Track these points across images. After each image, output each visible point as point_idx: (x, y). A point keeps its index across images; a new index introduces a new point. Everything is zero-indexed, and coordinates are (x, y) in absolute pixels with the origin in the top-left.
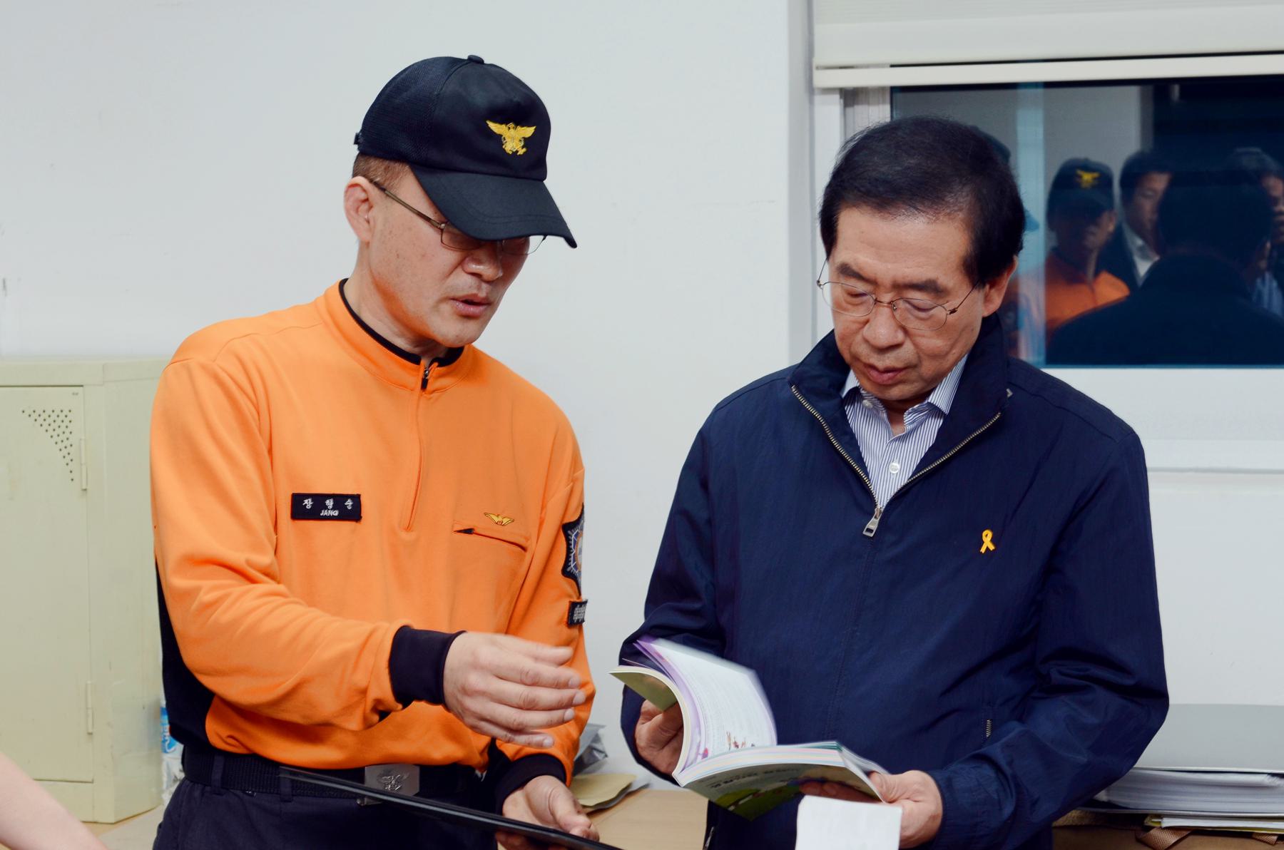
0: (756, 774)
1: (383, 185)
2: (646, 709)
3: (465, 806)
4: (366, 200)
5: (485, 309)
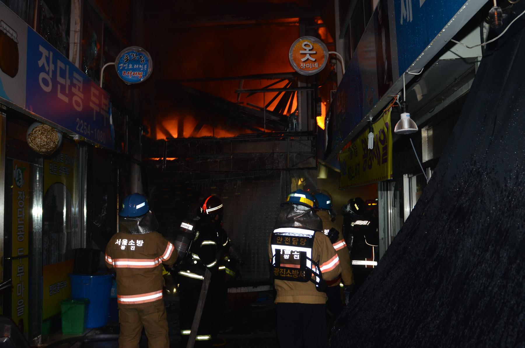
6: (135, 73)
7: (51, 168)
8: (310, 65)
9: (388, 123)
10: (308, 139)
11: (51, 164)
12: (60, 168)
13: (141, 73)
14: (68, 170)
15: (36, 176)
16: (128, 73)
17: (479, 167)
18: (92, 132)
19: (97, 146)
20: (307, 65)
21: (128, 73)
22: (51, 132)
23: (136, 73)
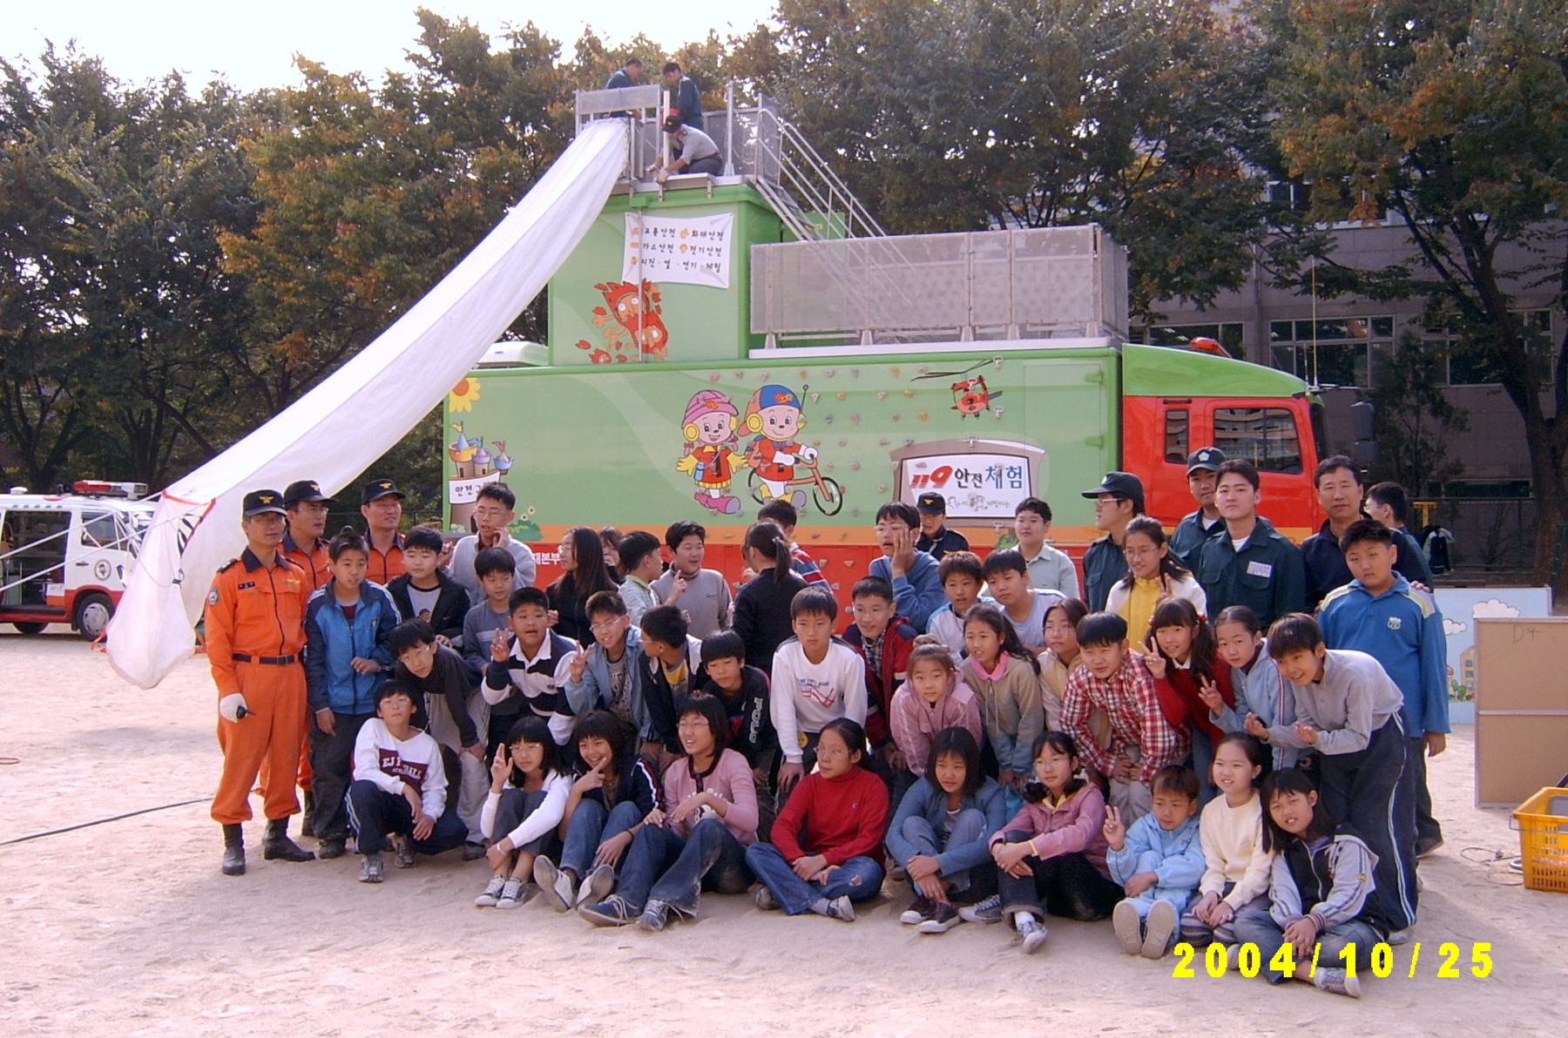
0: (934, 642)
1: (1179, 905)
2: (578, 708)
3: (1365, 903)
4: (237, 657)
5: (997, 547)
9: (937, 894)
10: (385, 83)
15: (1093, 620)
17: (1083, 187)
20: (264, 149)
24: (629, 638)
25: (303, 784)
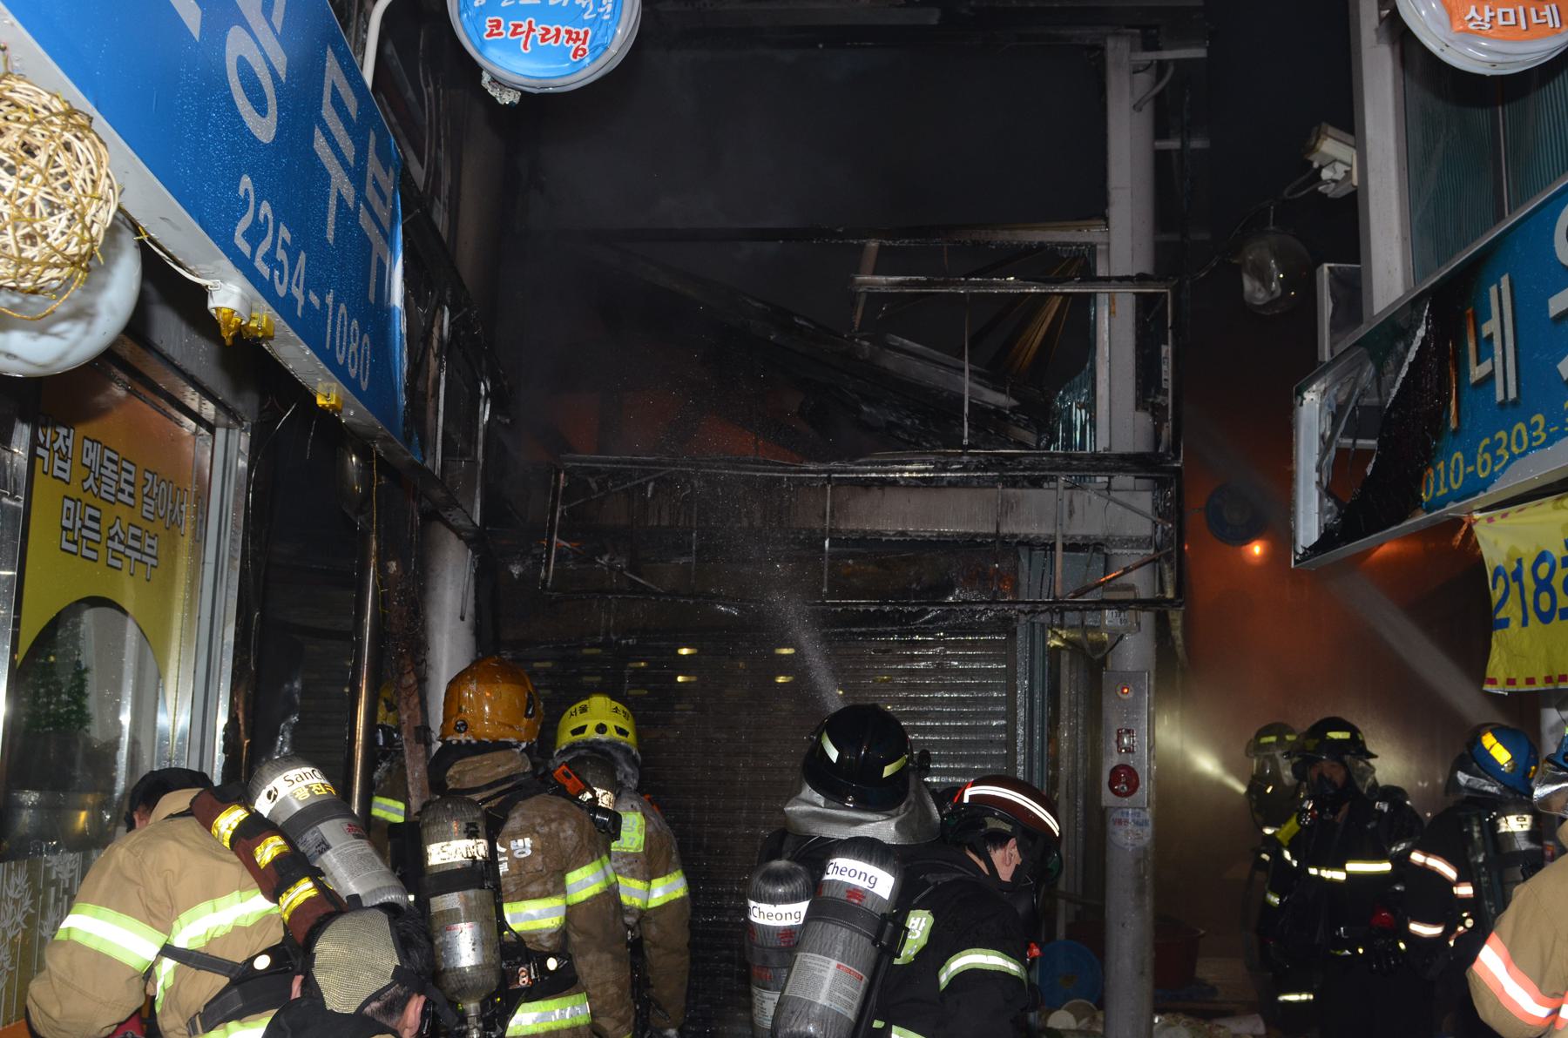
6: (553, 32)
7: (69, 524)
8: (1516, 13)
11: (68, 503)
12: (112, 532)
13: (582, 36)
14: (150, 546)
16: (517, 26)
18: (314, 299)
19: (327, 397)
21: (517, 26)
22: (58, 130)
23: (558, 31)
24: (888, 351)
25: (476, 541)
